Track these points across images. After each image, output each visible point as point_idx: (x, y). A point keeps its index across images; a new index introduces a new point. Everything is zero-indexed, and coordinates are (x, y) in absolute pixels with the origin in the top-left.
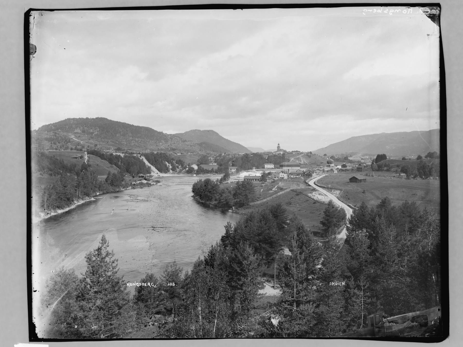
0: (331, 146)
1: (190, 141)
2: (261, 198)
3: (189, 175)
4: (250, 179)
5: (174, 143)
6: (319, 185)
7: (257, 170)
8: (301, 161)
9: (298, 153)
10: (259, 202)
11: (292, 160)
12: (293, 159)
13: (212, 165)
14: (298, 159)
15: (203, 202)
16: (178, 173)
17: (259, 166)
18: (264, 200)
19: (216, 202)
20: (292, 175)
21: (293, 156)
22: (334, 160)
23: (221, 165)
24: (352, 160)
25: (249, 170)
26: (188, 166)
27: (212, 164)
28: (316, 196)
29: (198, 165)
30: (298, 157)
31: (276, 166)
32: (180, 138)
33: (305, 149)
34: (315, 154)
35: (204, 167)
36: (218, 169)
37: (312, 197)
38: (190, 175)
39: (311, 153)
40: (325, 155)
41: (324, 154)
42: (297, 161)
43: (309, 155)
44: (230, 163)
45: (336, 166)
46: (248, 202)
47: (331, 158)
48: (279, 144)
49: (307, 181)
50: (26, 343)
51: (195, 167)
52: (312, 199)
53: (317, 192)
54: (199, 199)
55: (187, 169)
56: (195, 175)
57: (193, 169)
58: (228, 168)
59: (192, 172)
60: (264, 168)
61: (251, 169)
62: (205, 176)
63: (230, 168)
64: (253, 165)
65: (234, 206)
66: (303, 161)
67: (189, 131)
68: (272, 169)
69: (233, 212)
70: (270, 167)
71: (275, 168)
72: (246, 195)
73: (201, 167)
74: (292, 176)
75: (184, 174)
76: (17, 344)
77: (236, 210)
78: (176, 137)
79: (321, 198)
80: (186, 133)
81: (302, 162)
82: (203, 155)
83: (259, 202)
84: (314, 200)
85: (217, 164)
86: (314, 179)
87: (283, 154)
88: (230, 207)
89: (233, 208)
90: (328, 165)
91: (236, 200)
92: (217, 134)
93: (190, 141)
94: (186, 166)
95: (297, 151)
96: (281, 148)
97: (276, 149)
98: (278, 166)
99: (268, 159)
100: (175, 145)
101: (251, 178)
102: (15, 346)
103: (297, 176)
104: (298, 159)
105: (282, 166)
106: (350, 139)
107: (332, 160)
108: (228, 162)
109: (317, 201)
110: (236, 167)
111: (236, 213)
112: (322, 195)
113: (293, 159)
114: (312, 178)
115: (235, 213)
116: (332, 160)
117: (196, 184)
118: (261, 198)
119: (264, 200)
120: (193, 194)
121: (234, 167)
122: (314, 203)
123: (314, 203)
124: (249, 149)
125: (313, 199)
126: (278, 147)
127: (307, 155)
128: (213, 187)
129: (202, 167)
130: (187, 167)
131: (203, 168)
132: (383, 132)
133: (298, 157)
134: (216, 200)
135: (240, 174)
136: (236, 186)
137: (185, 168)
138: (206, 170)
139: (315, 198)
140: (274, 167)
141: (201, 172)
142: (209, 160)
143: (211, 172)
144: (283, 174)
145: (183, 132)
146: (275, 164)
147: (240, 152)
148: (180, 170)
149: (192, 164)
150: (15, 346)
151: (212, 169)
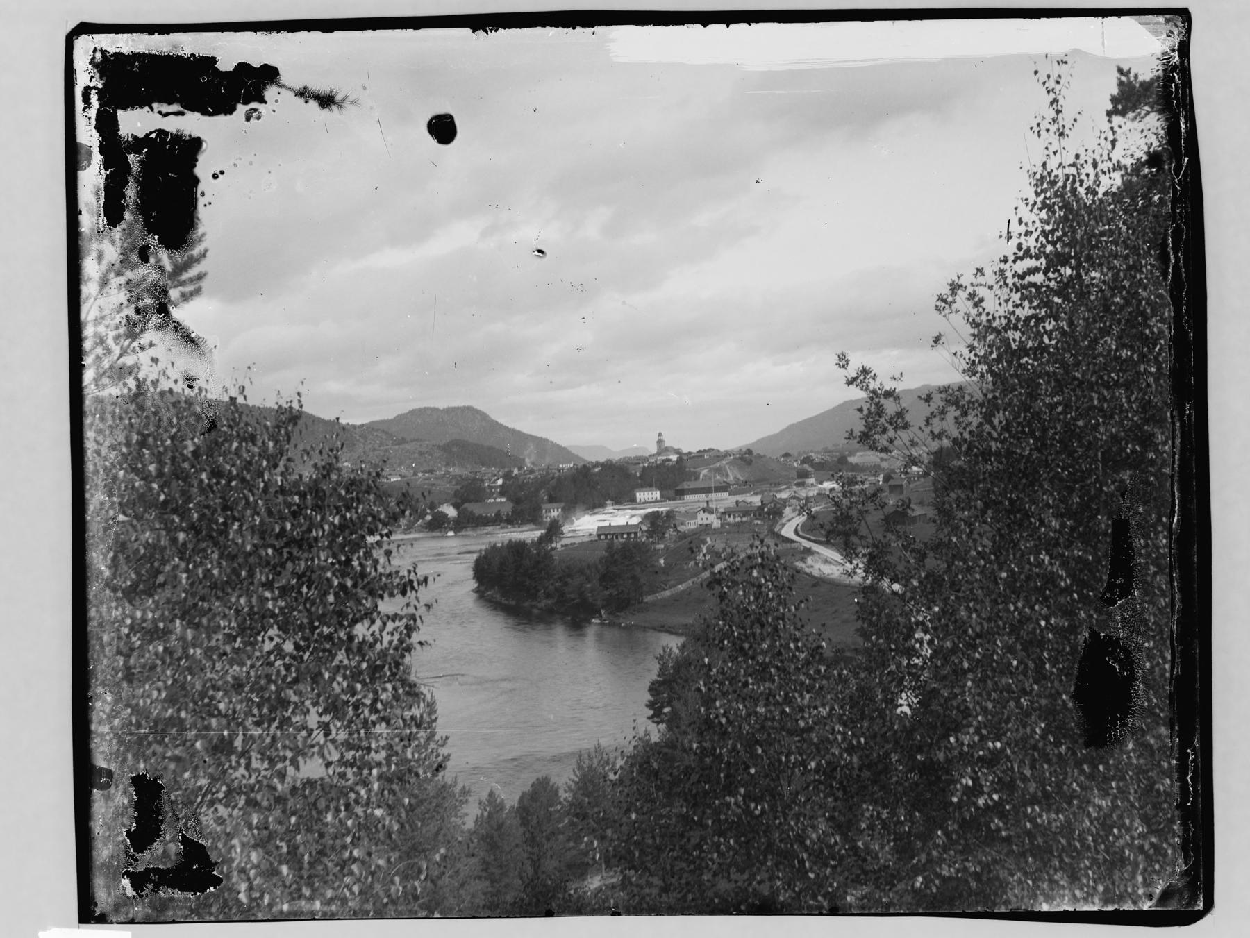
0: (791, 428)
1: (418, 440)
2: (672, 582)
3: (434, 534)
4: (613, 535)
5: (374, 450)
6: (812, 538)
7: (617, 507)
8: (727, 475)
9: (719, 456)
10: (667, 593)
11: (705, 476)
12: (705, 472)
13: (495, 502)
14: (719, 470)
15: (513, 603)
16: (406, 531)
17: (623, 497)
18: (681, 587)
19: (550, 602)
20: (729, 516)
21: (706, 463)
22: (812, 466)
23: (517, 501)
24: (857, 464)
25: (596, 510)
26: (428, 511)
27: (492, 500)
28: (817, 566)
29: (456, 506)
30: (718, 464)
31: (665, 492)
32: (386, 433)
33: (731, 439)
34: (759, 456)
35: (476, 509)
36: (513, 512)
37: (807, 570)
38: (439, 534)
39: (750, 452)
40: (787, 455)
41: (783, 453)
42: (718, 477)
43: (746, 458)
44: (543, 495)
45: (821, 483)
46: (641, 595)
47: (803, 462)
48: (660, 434)
49: (776, 530)
50: (70, 927)
51: (451, 512)
52: (807, 574)
53: (816, 557)
54: (498, 597)
55: (429, 518)
56: (451, 533)
57: (445, 515)
58: (540, 509)
59: (443, 524)
60: (633, 500)
61: (603, 505)
62: (479, 532)
63: (545, 506)
64: (607, 496)
65: (603, 607)
66: (733, 475)
67: (407, 414)
68: (656, 501)
69: (602, 624)
70: (650, 496)
71: (664, 498)
72: (634, 578)
73: (466, 509)
74: (731, 520)
75: (420, 531)
76: (45, 929)
77: (611, 617)
78: (377, 430)
79: (830, 572)
80: (399, 419)
81: (731, 479)
82: (461, 476)
83: (667, 593)
84: (814, 577)
85: (509, 499)
86: (789, 524)
87: (680, 460)
88: (593, 611)
89: (603, 612)
90: (800, 481)
91: (607, 593)
92: (484, 416)
93: (418, 440)
94: (424, 510)
95: (710, 450)
96: (667, 444)
97: (654, 450)
98: (671, 493)
99: (641, 477)
100: (376, 453)
101: (617, 531)
102: (41, 934)
103: (744, 519)
104: (719, 470)
105: (681, 493)
106: (840, 406)
107: (810, 469)
108: (537, 491)
109: (820, 578)
110: (563, 504)
111: (612, 625)
112: (830, 563)
113: (705, 472)
114: (784, 520)
115: (609, 625)
116: (810, 469)
117: (485, 557)
118: (672, 582)
119: (681, 587)
120: (476, 585)
121: (555, 505)
122: (814, 585)
123: (814, 585)
124: (574, 452)
125: (810, 575)
126: (660, 442)
127: (742, 458)
128: (538, 562)
129: (470, 509)
130: (427, 514)
131: (472, 513)
132: (926, 383)
133: (718, 464)
134: (548, 596)
135: (572, 522)
136: (606, 554)
137: (423, 515)
138: (481, 516)
139: (816, 573)
140: (662, 496)
141: (468, 522)
142: (484, 489)
143: (496, 521)
144: (706, 515)
145: (391, 417)
146: (661, 488)
147: (560, 463)
148: (410, 521)
149: (441, 504)
150: (41, 934)
151: (498, 514)
